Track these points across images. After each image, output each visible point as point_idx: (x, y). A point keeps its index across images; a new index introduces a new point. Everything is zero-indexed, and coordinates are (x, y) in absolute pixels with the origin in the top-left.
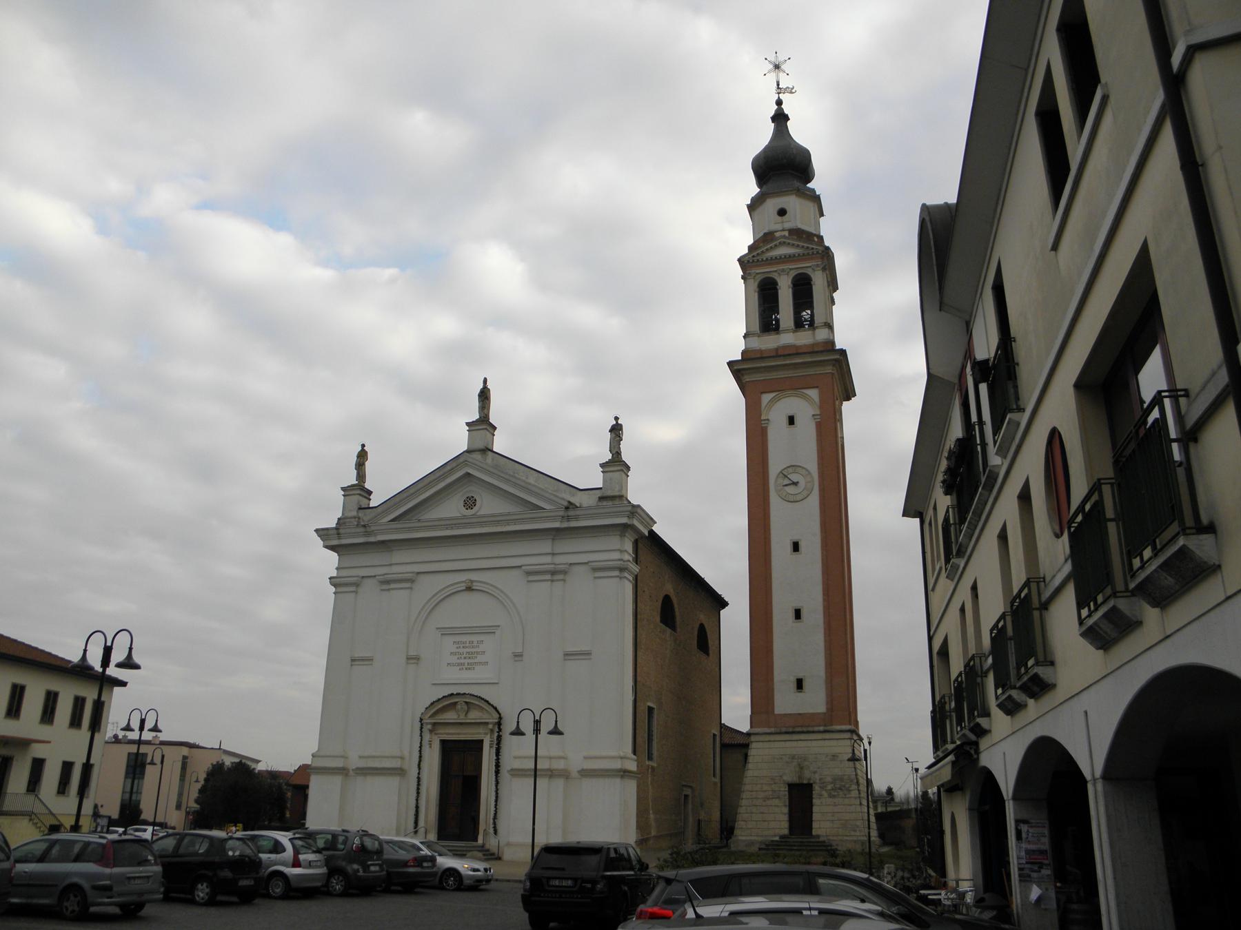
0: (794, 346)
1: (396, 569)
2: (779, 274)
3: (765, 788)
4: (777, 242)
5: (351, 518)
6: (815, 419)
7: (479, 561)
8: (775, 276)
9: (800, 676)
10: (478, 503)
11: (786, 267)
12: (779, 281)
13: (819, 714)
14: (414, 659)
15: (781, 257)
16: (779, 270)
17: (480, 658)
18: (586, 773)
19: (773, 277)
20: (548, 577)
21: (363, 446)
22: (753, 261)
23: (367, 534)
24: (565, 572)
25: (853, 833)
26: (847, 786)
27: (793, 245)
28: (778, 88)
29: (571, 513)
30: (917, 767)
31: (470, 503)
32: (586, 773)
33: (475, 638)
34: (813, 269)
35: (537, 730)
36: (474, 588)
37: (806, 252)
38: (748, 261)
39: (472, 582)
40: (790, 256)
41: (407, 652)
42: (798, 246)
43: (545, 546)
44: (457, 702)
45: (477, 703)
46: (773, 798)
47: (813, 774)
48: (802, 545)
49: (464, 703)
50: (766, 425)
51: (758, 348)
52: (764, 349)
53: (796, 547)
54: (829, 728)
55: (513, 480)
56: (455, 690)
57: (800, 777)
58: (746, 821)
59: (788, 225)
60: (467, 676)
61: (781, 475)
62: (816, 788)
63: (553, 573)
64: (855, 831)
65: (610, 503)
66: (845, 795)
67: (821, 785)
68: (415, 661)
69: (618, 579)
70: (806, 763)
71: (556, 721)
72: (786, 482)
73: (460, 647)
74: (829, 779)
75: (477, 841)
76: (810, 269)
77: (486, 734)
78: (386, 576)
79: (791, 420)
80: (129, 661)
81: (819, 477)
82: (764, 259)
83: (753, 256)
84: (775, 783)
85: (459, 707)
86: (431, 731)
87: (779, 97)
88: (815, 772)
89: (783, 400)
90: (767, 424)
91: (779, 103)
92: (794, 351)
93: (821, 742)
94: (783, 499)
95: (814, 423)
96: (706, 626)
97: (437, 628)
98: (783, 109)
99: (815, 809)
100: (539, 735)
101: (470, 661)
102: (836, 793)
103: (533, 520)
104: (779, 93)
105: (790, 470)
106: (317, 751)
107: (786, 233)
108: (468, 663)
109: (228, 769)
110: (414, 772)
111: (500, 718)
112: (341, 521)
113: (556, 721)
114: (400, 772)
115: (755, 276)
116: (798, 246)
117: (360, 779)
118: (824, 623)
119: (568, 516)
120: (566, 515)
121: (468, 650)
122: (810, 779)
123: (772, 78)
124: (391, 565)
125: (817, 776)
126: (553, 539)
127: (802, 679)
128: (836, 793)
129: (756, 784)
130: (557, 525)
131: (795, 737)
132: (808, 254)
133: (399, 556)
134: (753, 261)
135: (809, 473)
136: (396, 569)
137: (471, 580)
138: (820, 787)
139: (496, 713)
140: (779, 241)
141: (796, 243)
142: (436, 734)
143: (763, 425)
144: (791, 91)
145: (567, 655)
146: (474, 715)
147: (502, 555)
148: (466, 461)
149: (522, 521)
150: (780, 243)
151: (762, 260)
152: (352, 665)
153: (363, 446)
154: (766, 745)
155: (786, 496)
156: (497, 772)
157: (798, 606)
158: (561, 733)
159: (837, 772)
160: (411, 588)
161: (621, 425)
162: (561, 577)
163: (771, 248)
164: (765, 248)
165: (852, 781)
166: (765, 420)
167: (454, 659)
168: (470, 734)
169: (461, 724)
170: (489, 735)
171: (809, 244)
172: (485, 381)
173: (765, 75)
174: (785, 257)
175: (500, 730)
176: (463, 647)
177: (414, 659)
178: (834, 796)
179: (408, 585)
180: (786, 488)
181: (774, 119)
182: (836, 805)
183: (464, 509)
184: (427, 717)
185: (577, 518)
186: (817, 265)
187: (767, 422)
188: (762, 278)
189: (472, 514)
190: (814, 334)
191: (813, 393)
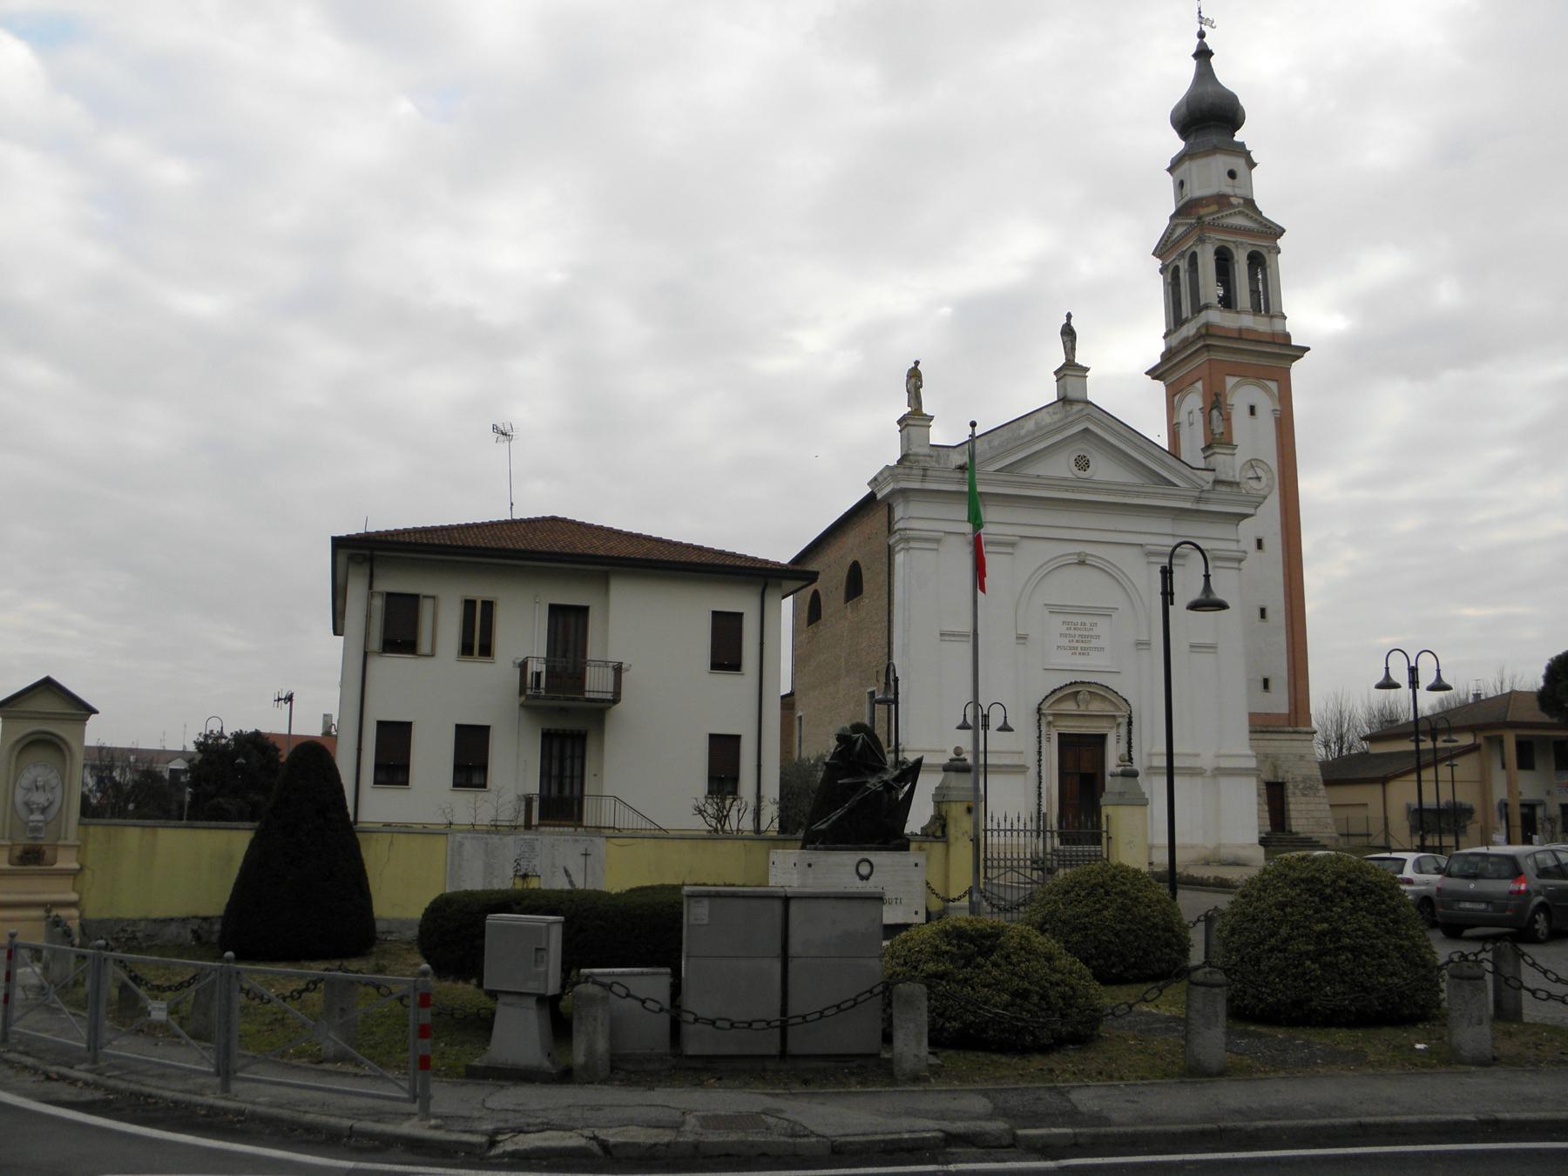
2: (1237, 246)
4: (1236, 210)
5: (924, 456)
7: (1104, 534)
8: (1232, 247)
10: (1091, 463)
12: (1267, 258)
14: (1022, 638)
15: (1236, 228)
17: (1094, 643)
21: (917, 363)
25: (1325, 830)
28: (1200, 16)
31: (1083, 463)
32: (1220, 772)
33: (1088, 620)
36: (1087, 562)
37: (1265, 230)
38: (1209, 223)
39: (1087, 555)
54: (1296, 729)
57: (1275, 776)
59: (1238, 192)
60: (1080, 662)
62: (1290, 788)
65: (1228, 489)
71: (1005, 717)
74: (1299, 779)
77: (1112, 728)
79: (1252, 410)
81: (1279, 475)
85: (1081, 697)
86: (1049, 723)
87: (1201, 28)
88: (1287, 772)
91: (1201, 35)
92: (1241, 335)
95: (1273, 419)
96: (821, 592)
97: (1045, 605)
98: (1205, 44)
101: (1083, 645)
104: (1201, 23)
107: (1241, 201)
108: (1081, 648)
109: (196, 782)
110: (1033, 771)
113: (1005, 717)
122: (1283, 779)
125: (1289, 776)
130: (1188, 505)
131: (1268, 736)
132: (1266, 232)
135: (1271, 470)
141: (1228, 213)
142: (1054, 726)
146: (1096, 707)
147: (1205, 535)
149: (1146, 495)
153: (917, 363)
154: (1289, 743)
157: (1263, 604)
158: (1011, 730)
166: (1230, 405)
167: (1065, 642)
169: (1083, 716)
170: (1115, 729)
172: (1069, 316)
175: (1130, 723)
176: (1075, 629)
180: (1250, 481)
181: (1196, 56)
190: (1271, 322)
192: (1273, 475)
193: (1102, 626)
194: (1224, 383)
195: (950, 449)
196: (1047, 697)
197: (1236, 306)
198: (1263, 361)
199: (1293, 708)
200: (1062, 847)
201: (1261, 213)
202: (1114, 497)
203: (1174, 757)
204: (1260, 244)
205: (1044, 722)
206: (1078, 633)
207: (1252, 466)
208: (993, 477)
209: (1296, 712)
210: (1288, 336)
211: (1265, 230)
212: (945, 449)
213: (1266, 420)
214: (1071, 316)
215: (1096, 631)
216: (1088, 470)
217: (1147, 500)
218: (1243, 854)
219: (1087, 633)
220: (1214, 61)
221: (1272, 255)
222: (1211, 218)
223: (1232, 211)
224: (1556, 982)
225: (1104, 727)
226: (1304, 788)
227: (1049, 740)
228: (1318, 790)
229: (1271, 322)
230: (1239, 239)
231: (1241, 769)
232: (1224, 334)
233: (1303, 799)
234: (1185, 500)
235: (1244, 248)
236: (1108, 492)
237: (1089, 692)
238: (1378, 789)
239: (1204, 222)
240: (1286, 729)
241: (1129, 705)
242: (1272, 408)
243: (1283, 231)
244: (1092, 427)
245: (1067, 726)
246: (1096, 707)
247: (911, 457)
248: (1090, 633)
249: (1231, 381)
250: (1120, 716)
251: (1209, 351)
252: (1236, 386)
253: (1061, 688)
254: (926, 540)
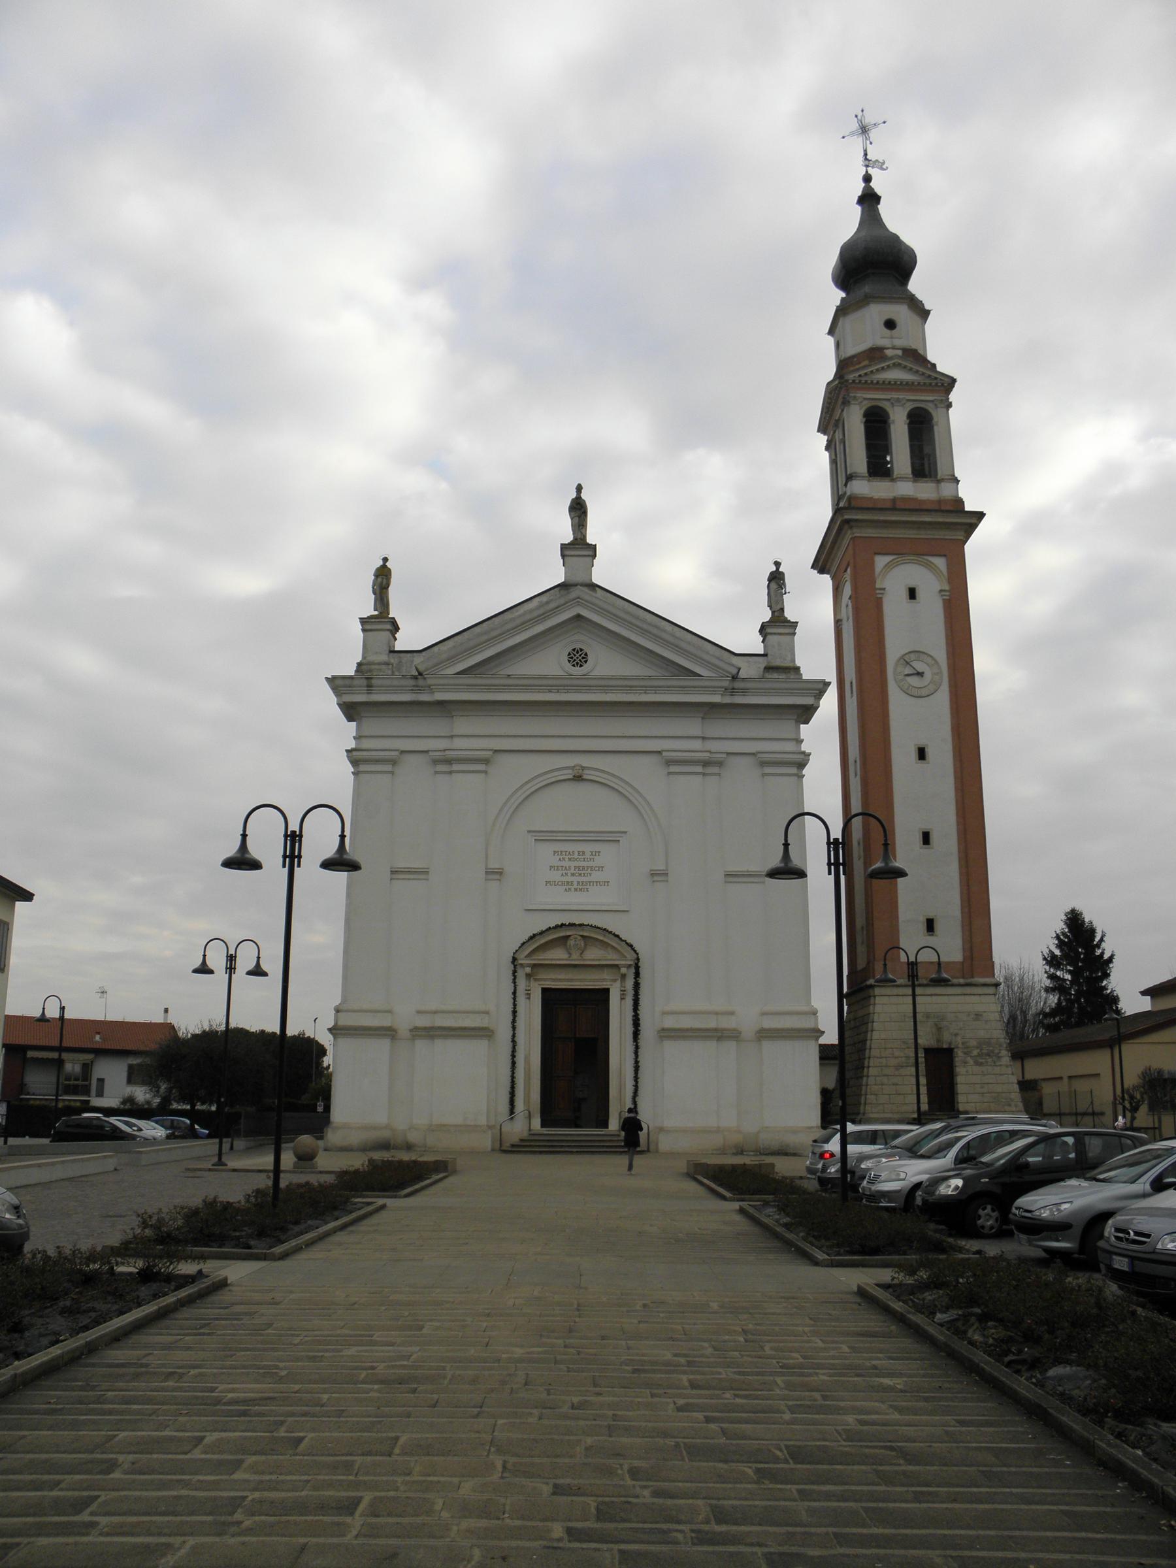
0: (915, 500)
1: (458, 743)
2: (936, 406)
3: (897, 1053)
4: (891, 362)
5: (379, 664)
6: (942, 596)
8: (886, 406)
9: (931, 916)
10: (590, 658)
11: (901, 396)
13: (954, 963)
14: (494, 874)
16: (937, 400)
17: (596, 876)
18: (765, 1034)
19: (927, 408)
20: (699, 769)
21: (385, 560)
22: (860, 381)
23: (417, 689)
24: (720, 764)
26: (996, 1051)
27: (911, 369)
28: (866, 159)
31: (578, 657)
32: (765, 1034)
33: (588, 848)
34: (936, 405)
35: (231, 968)
36: (585, 777)
37: (928, 381)
38: (854, 381)
39: (583, 768)
40: (907, 383)
41: (486, 865)
42: (917, 372)
43: (693, 726)
44: (570, 936)
45: (601, 938)
46: (907, 1066)
47: (954, 1037)
48: (930, 752)
49: (579, 938)
50: (880, 596)
51: (870, 496)
52: (877, 497)
53: (922, 754)
54: (969, 981)
55: (655, 631)
56: (566, 919)
57: (938, 1041)
58: (876, 1095)
59: (898, 343)
60: (576, 900)
61: (902, 661)
62: (959, 1055)
63: (706, 763)
64: (1010, 1105)
65: (783, 676)
66: (995, 1062)
67: (965, 1050)
68: (497, 877)
69: (796, 778)
70: (945, 1023)
72: (908, 671)
73: (564, 859)
74: (973, 1043)
75: (607, 1128)
76: (930, 405)
77: (615, 980)
78: (447, 752)
79: (912, 594)
80: (786, 864)
81: (949, 668)
82: (875, 382)
83: (860, 376)
84: (908, 1048)
85: (571, 942)
86: (528, 976)
87: (867, 172)
88: (956, 1035)
89: (902, 567)
90: (882, 594)
91: (867, 179)
92: (895, 505)
93: (960, 997)
94: (904, 691)
97: (529, 832)
99: (960, 1079)
100: (233, 975)
101: (581, 879)
102: (983, 1061)
103: (683, 689)
104: (867, 166)
105: (913, 656)
106: (340, 1004)
107: (900, 353)
108: (578, 882)
110: (504, 1033)
111: (638, 959)
112: (364, 667)
114: (667, 1034)
115: (862, 402)
116: (917, 372)
117: (420, 1044)
118: (959, 852)
119: (733, 689)
120: (731, 687)
121: (577, 864)
122: (950, 1044)
123: (858, 143)
124: (452, 737)
125: (959, 1040)
126: (703, 718)
128: (983, 1061)
129: (885, 1048)
130: (717, 699)
133: (463, 725)
134: (860, 381)
136: (458, 743)
137: (582, 767)
138: (965, 1053)
139: (632, 952)
140: (892, 362)
142: (536, 980)
144: (881, 166)
145: (730, 876)
146: (594, 955)
148: (578, 598)
150: (894, 364)
151: (872, 382)
152: (486, 880)
153: (385, 560)
154: (894, 1000)
155: (908, 689)
156: (636, 1034)
157: (926, 828)
159: (982, 1034)
160: (486, 772)
161: (782, 574)
162: (715, 770)
163: (883, 368)
164: (917, 368)
165: (1001, 1045)
166: (880, 589)
167: (556, 876)
168: (591, 980)
169: (575, 966)
170: (619, 982)
172: (579, 488)
173: (843, 137)
174: (901, 383)
175: (637, 974)
176: (570, 859)
177: (494, 874)
178: (981, 1064)
179: (482, 767)
180: (909, 679)
181: (862, 200)
182: (984, 1075)
183: (569, 665)
184: (522, 956)
186: (942, 400)
188: (869, 405)
189: (580, 673)
190: (938, 488)
192: (939, 667)
193: (607, 855)
194: (872, 564)
195: (415, 654)
196: (523, 944)
197: (893, 473)
198: (923, 534)
200: (545, 1131)
201: (934, 366)
202: (614, 695)
204: (925, 399)
205: (521, 974)
206: (573, 864)
207: (908, 663)
208: (451, 682)
209: (972, 959)
210: (960, 502)
211: (928, 381)
212: (409, 655)
213: (931, 606)
214: (582, 488)
215: (598, 861)
216: (585, 666)
217: (657, 695)
218: (793, 1140)
219: (585, 864)
220: (882, 208)
221: (939, 410)
222: (857, 375)
223: (916, 367)
225: (604, 980)
226: (979, 1055)
227: (528, 996)
228: (999, 1058)
229: (938, 488)
230: (895, 395)
231: (792, 1030)
232: (870, 506)
233: (977, 1069)
234: (714, 693)
235: (903, 405)
236: (605, 689)
237: (582, 936)
239: (847, 381)
241: (635, 951)
242: (939, 588)
243: (953, 381)
244: (585, 613)
245: (554, 980)
246: (594, 955)
248: (590, 864)
249: (881, 561)
250: (624, 966)
251: (851, 528)
253: (542, 933)
254: (377, 761)
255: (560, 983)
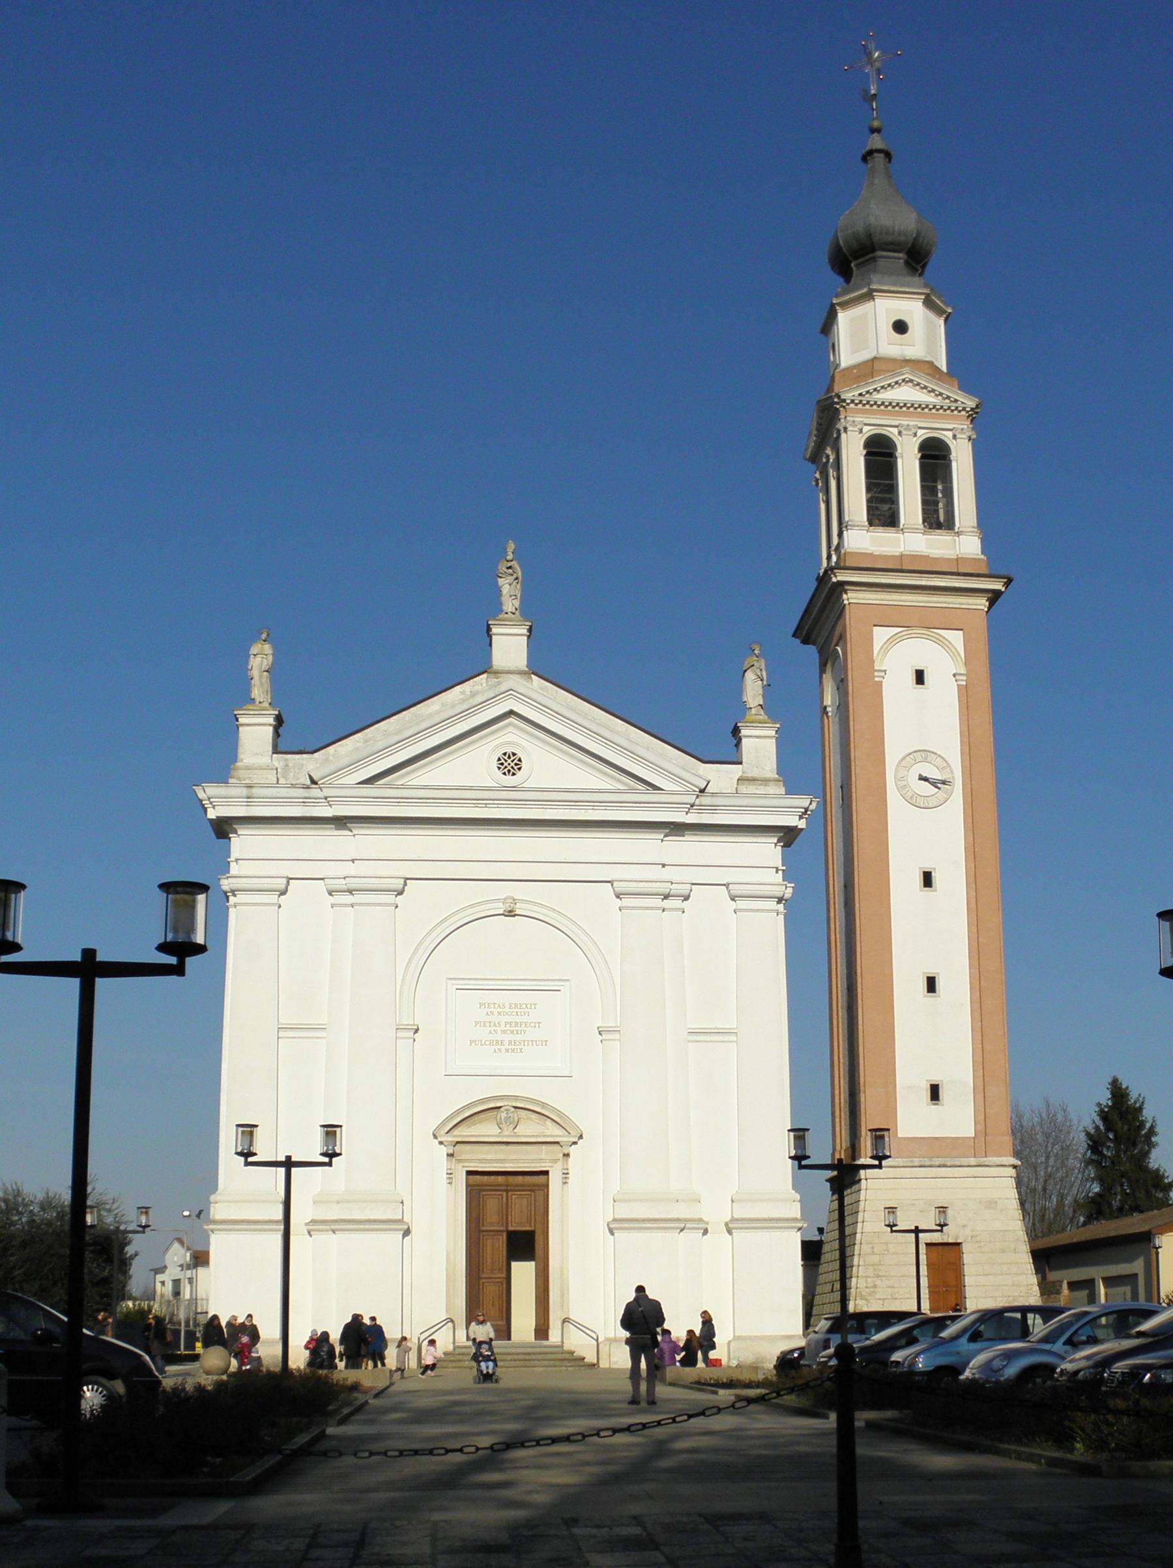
29: (705, 800)
30: (162, 1280)
31: (510, 763)
38: (852, 401)
48: (936, 878)
50: (881, 679)
54: (983, 1160)
75: (547, 1339)
76: (950, 434)
77: (555, 1161)
83: (860, 395)
127: (938, 1085)
141: (924, 383)
142: (460, 1161)
143: (876, 679)
146: (529, 1129)
171: (937, 385)
176: (499, 1013)
183: (499, 773)
185: (713, 808)
187: (883, 674)
191: (956, 638)
197: (899, 522)
199: (981, 1127)
203: (274, 1168)
216: (519, 774)
219: (518, 1019)
222: (857, 393)
224: (370, 1456)
238: (736, 1216)
240: (965, 1161)
247: (241, 772)
252: (892, 642)
255: (488, 1165)
